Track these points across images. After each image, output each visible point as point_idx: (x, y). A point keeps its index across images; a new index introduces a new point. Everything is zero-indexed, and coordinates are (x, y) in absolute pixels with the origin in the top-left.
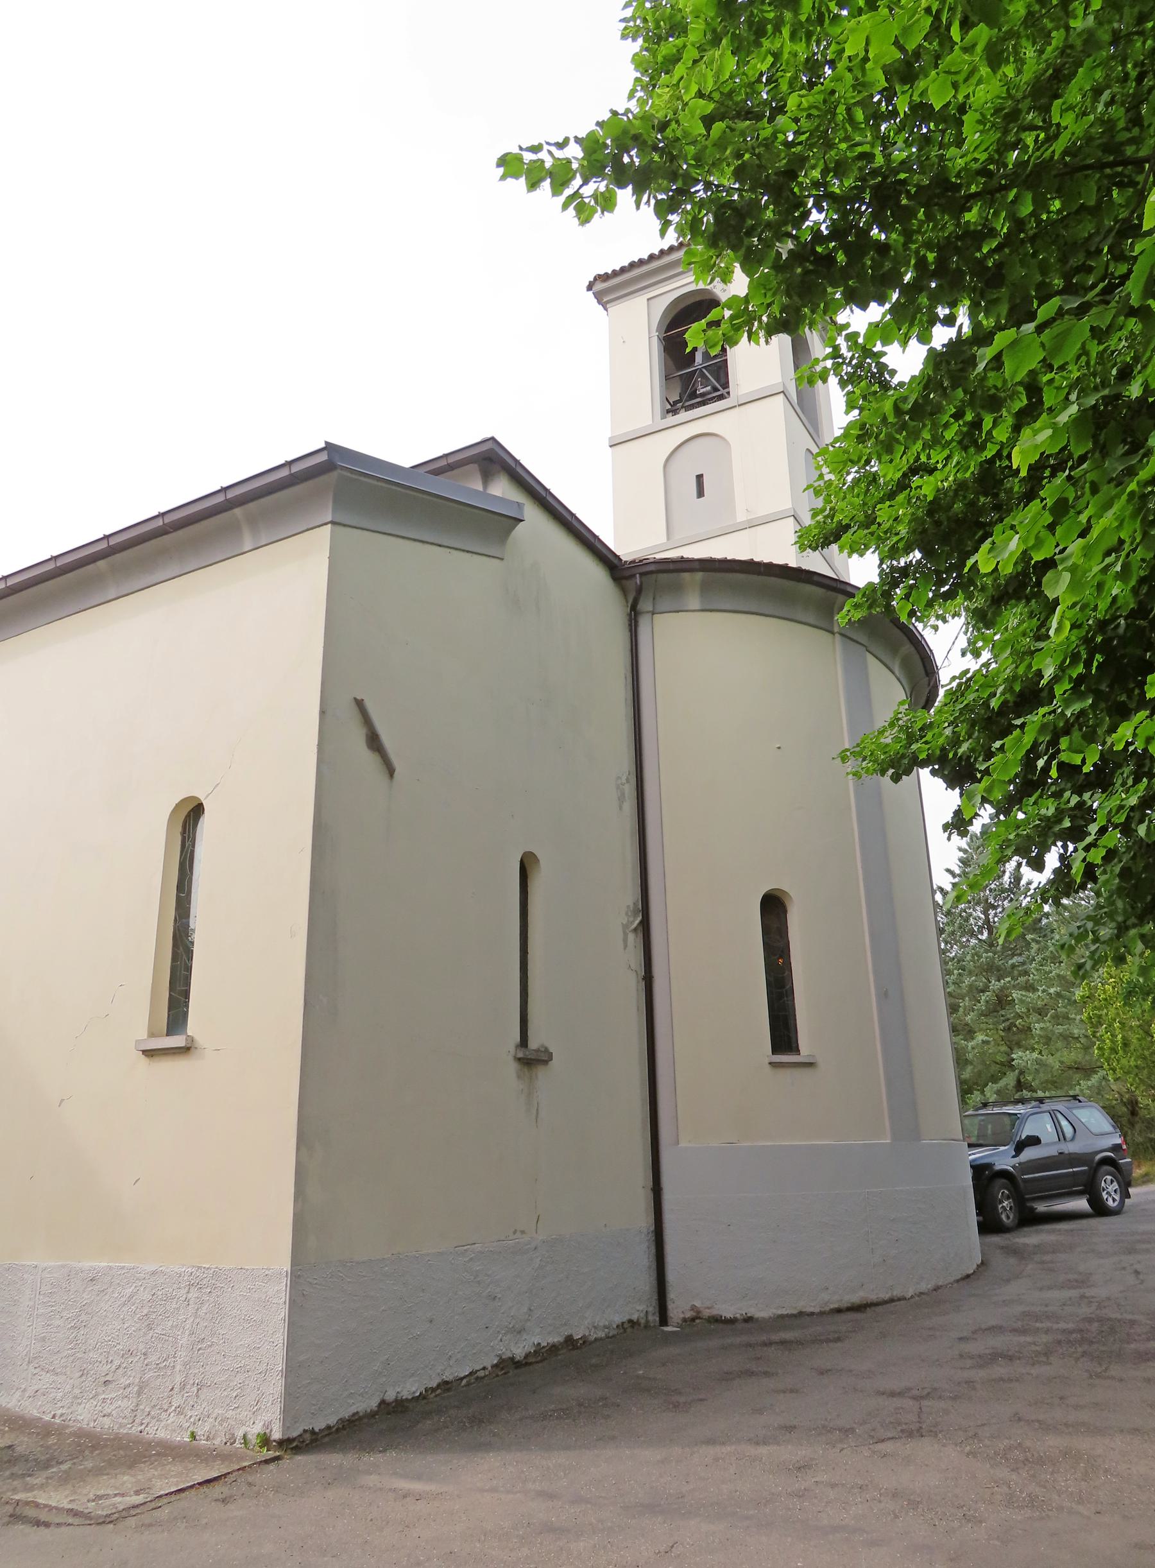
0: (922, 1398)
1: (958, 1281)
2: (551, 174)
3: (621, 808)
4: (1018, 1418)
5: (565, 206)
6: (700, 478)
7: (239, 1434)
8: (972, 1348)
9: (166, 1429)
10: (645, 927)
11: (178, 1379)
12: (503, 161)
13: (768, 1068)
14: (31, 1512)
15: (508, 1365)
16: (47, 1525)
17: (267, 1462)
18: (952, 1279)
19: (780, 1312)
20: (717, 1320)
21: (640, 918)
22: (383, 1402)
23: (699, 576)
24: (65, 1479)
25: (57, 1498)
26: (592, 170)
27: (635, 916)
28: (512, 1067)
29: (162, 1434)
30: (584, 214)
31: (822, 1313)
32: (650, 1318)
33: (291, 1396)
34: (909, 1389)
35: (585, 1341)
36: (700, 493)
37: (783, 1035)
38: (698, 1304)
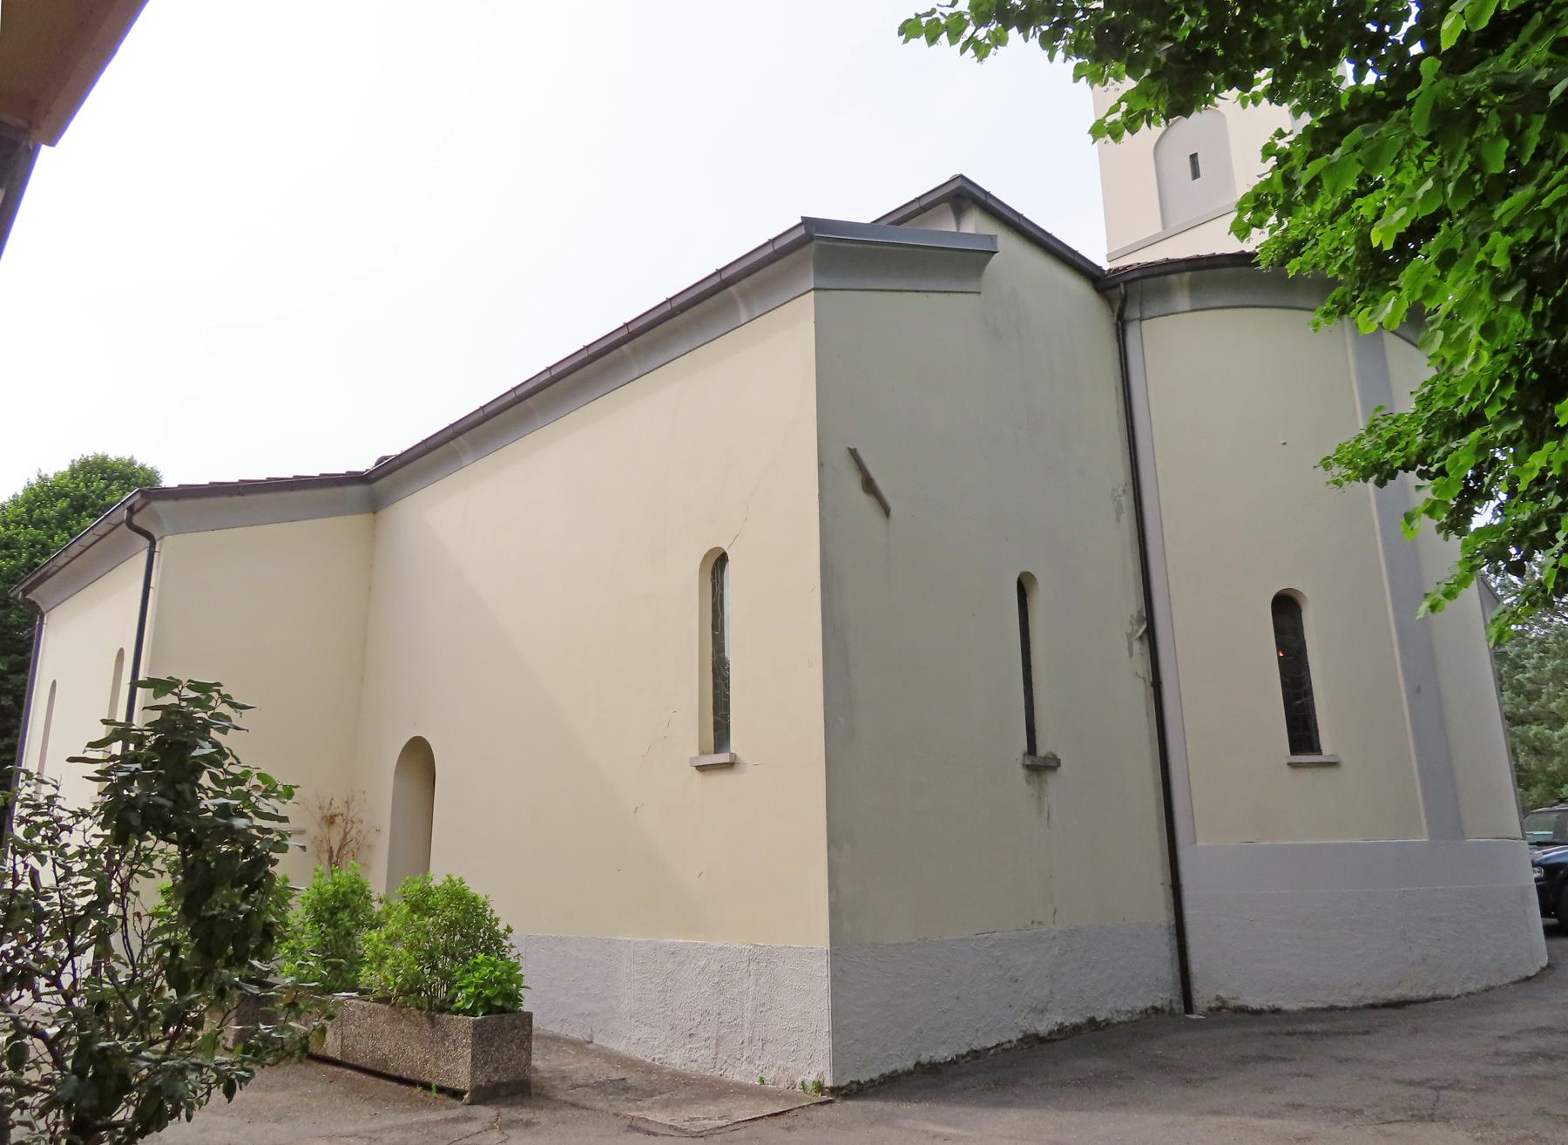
0: (1442, 1088)
1: (1515, 983)
2: (946, 27)
3: (1118, 519)
4: (1542, 1112)
5: (963, 51)
6: (1194, 157)
7: (799, 1081)
8: (1512, 1046)
9: (739, 1074)
10: (1150, 636)
11: (747, 1034)
12: (903, 29)
13: (1287, 770)
14: (644, 1126)
15: (1032, 1040)
16: (655, 1134)
17: (822, 1104)
18: (1507, 981)
19: (1310, 1005)
20: (1242, 1010)
21: (1145, 626)
22: (918, 1064)
23: (1187, 276)
24: (666, 1105)
25: (660, 1117)
26: (981, 21)
27: (1139, 623)
28: (1021, 774)
29: (737, 1078)
30: (981, 50)
31: (1355, 1009)
32: (1175, 1006)
33: (838, 1052)
34: (1429, 1080)
35: (1108, 1023)
36: (1196, 174)
37: (1303, 734)
38: (1223, 995)
